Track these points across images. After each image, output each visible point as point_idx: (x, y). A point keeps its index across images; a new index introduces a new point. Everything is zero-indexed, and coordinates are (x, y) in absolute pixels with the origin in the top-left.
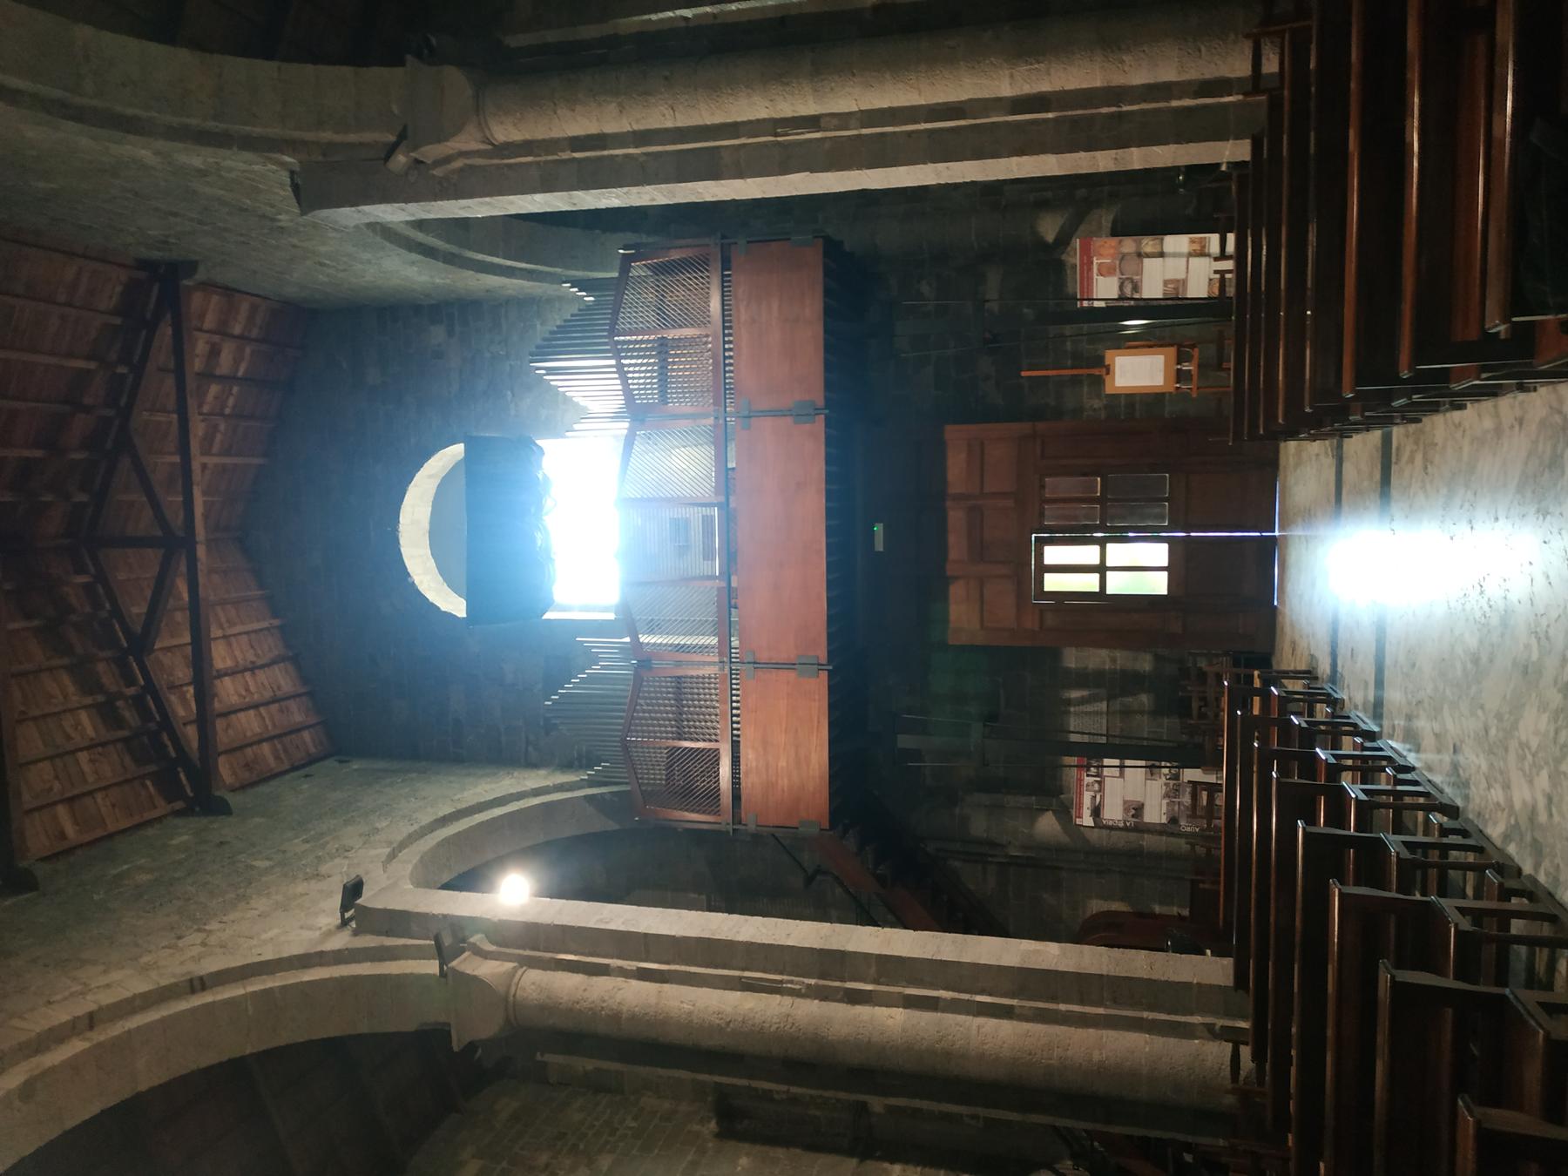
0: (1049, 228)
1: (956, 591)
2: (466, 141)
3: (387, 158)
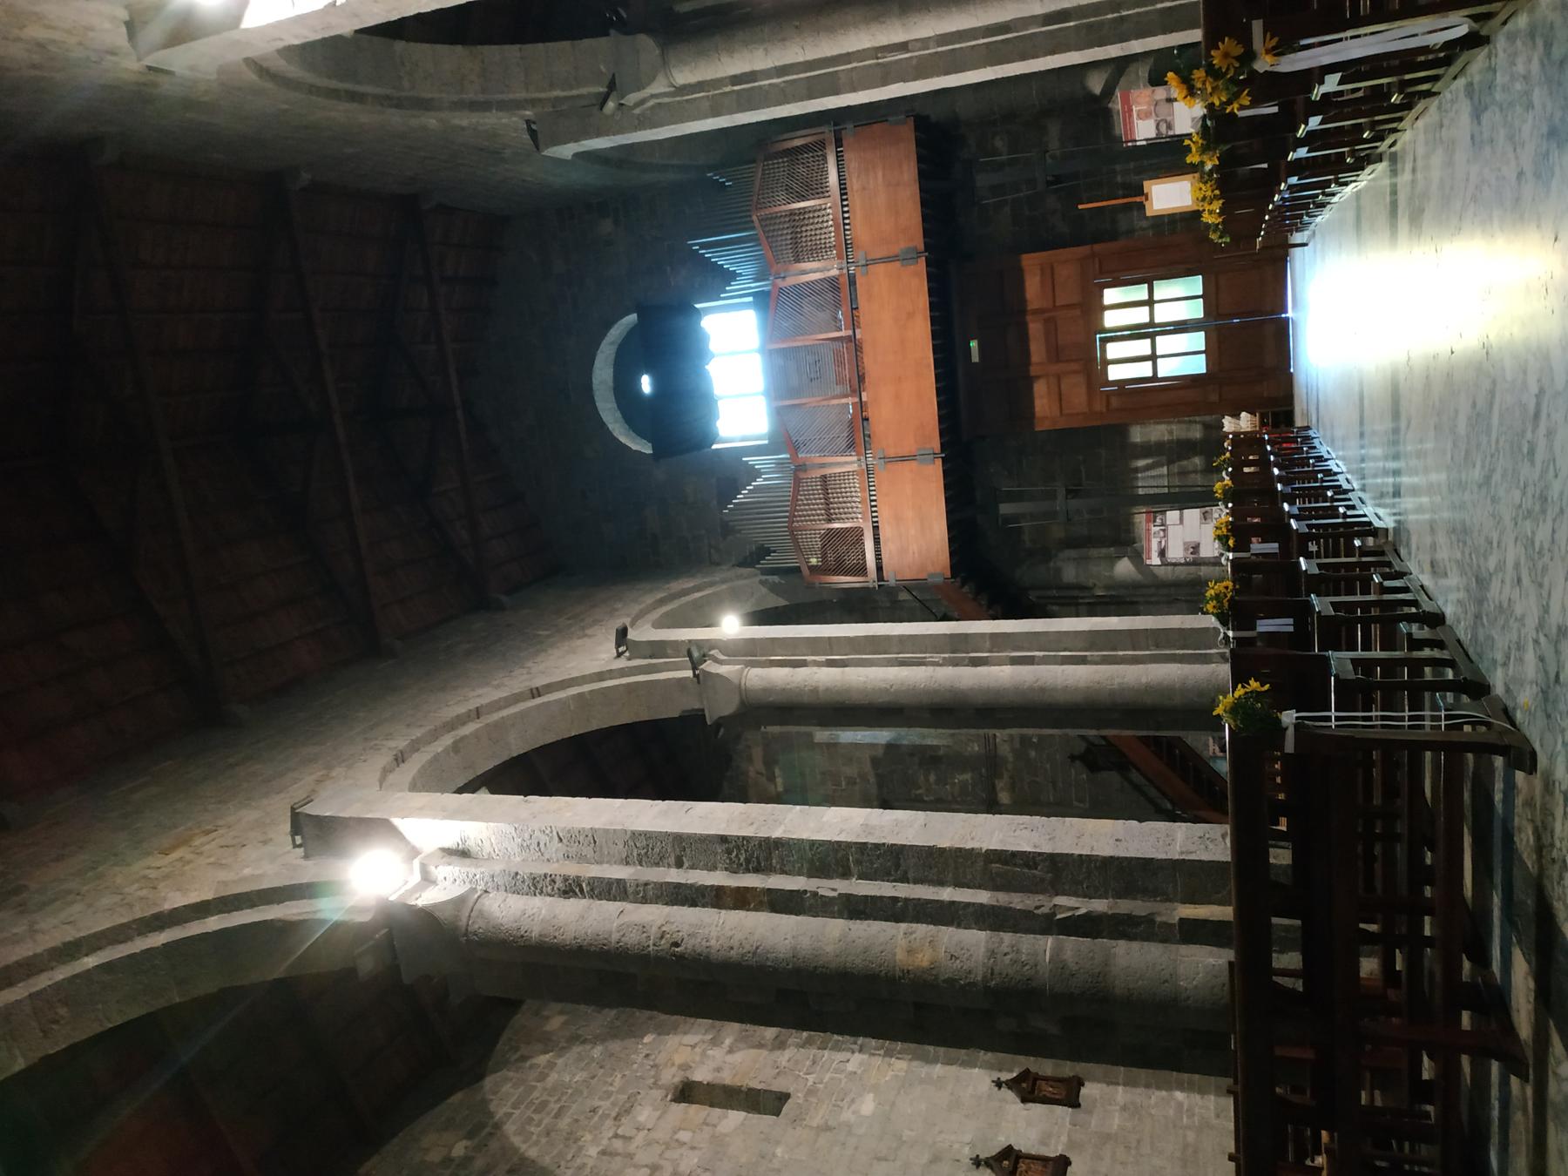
0: (1096, 84)
1: (1040, 389)
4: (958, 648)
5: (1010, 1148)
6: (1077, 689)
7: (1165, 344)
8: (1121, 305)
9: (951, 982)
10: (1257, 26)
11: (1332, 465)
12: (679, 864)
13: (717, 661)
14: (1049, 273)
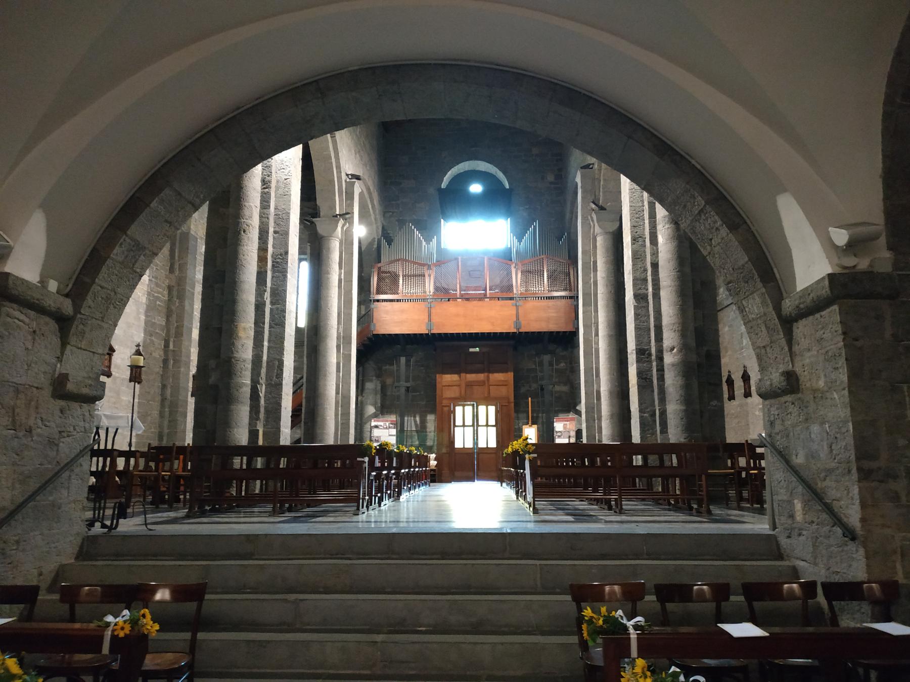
1: (455, 377)
2: (597, 229)
3: (593, 202)
4: (344, 339)
5: (114, 351)
6: (325, 390)
7: (469, 431)
8: (488, 413)
9: (233, 344)
10: (536, 455)
11: (417, 490)
12: (275, 232)
13: (343, 226)
14: (504, 384)
